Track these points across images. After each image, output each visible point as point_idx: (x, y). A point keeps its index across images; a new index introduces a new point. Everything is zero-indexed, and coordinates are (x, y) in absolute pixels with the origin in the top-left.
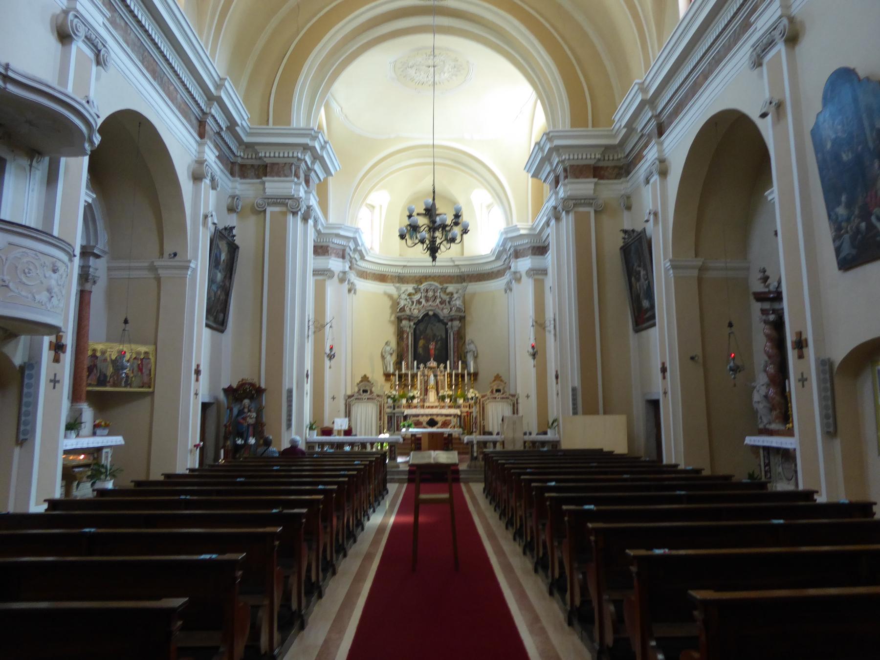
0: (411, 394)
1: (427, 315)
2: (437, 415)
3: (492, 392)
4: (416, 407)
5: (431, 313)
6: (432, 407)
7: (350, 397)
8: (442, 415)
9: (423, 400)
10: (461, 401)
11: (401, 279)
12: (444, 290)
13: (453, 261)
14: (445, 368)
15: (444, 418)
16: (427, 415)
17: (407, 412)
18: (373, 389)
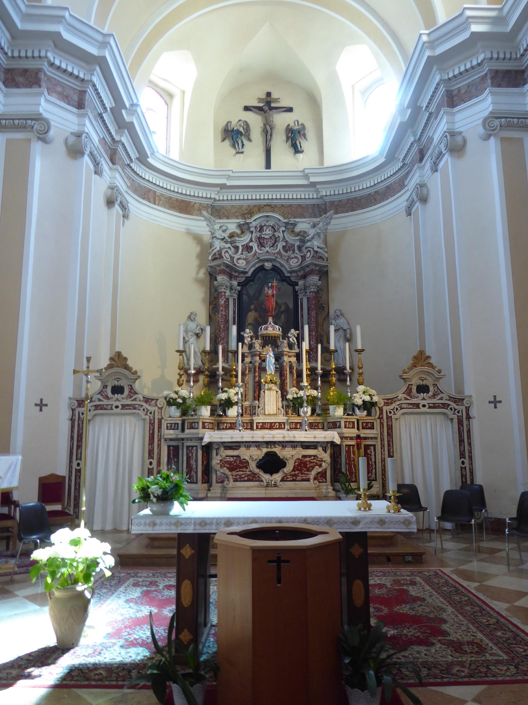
0: (223, 396)
1: (262, 268)
2: (283, 444)
3: (409, 392)
4: (232, 426)
5: (268, 265)
6: (271, 426)
7: (81, 403)
8: (294, 444)
9: (252, 411)
10: (338, 412)
11: (217, 211)
12: (290, 227)
13: (306, 177)
14: (300, 339)
15: (299, 452)
16: (258, 444)
17: (210, 436)
18: (137, 386)
